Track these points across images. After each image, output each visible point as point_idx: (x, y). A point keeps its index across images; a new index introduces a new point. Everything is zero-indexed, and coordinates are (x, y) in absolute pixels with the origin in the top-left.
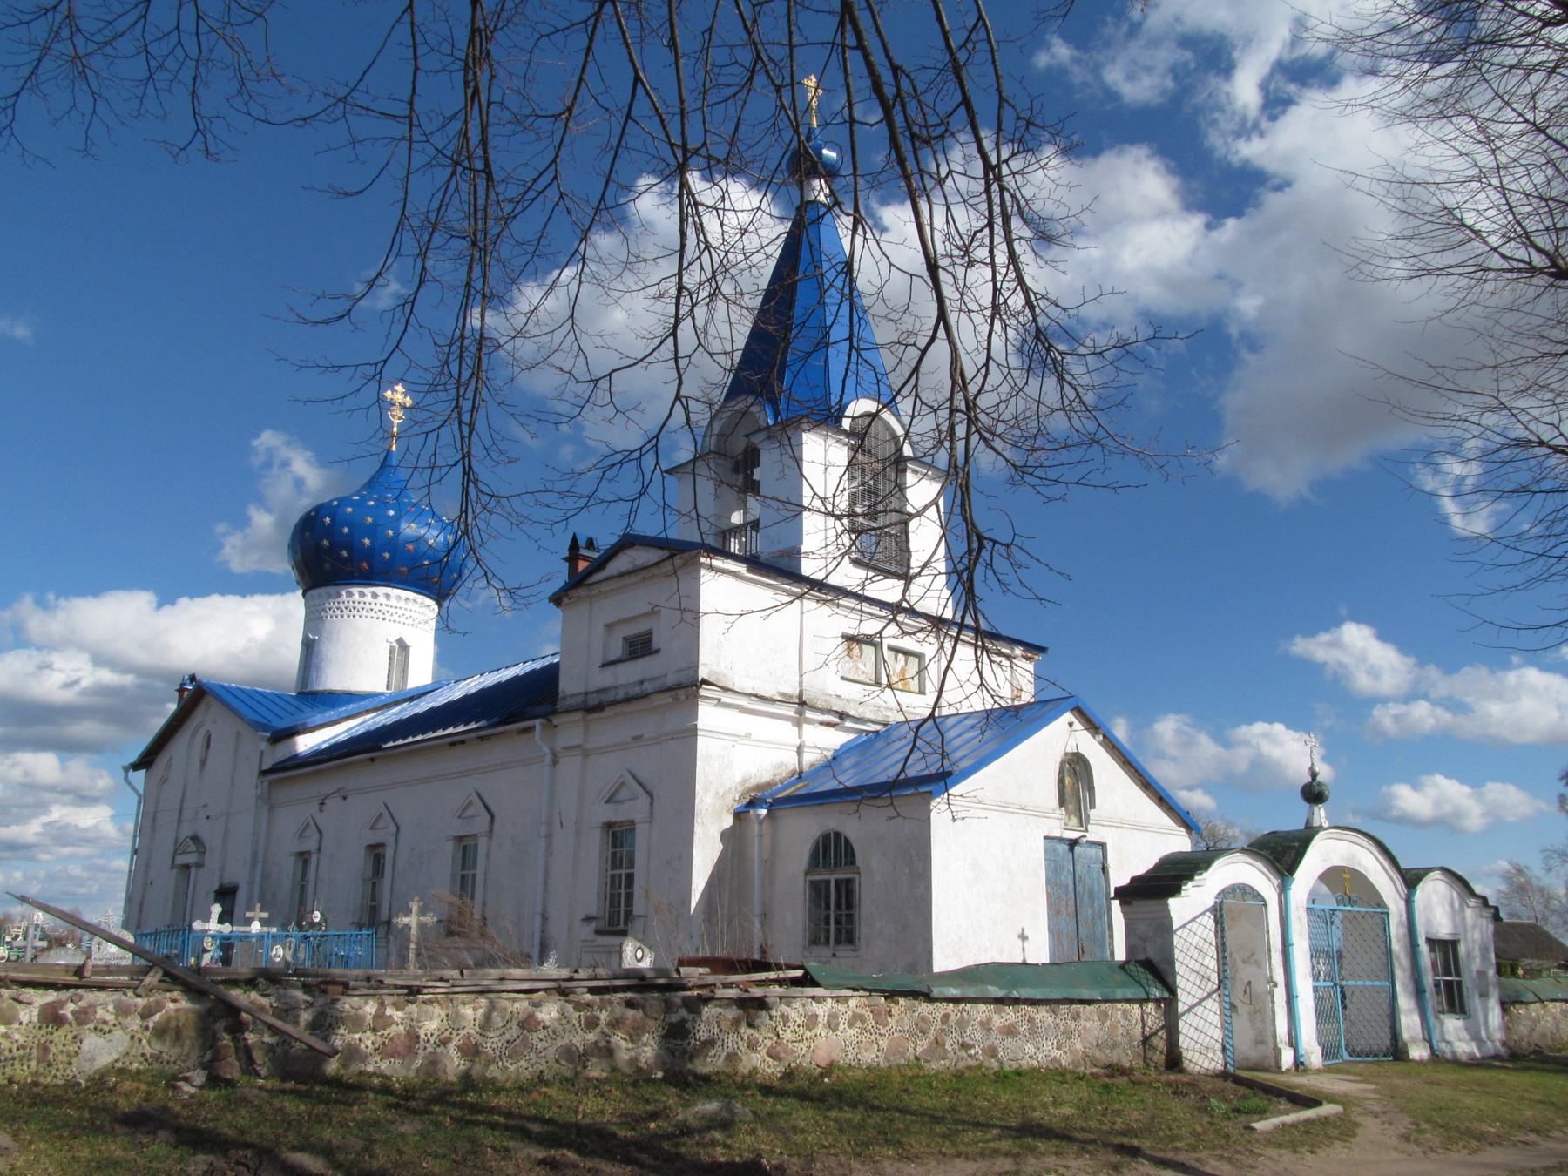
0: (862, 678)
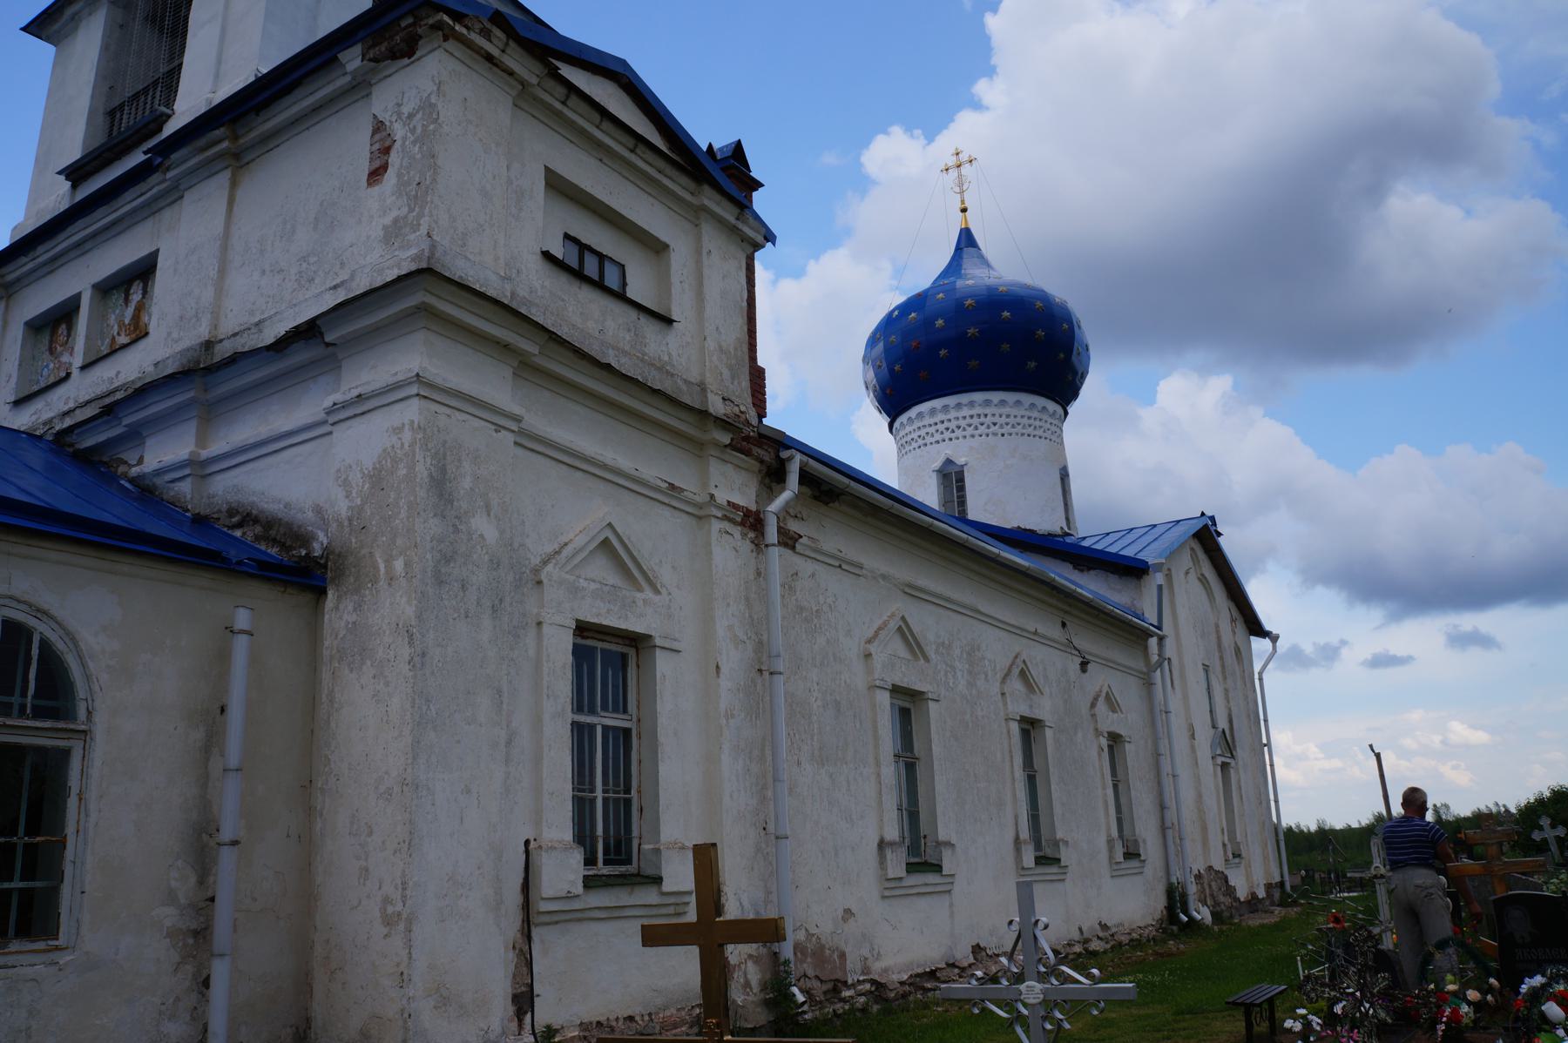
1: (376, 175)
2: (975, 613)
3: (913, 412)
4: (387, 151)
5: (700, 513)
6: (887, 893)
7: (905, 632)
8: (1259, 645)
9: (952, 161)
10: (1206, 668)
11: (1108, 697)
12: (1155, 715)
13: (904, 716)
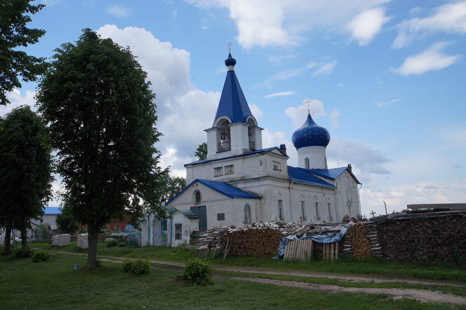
1: (261, 165)
2: (310, 191)
3: (301, 149)
5: (285, 188)
7: (303, 195)
8: (359, 186)
10: (347, 191)
13: (302, 204)
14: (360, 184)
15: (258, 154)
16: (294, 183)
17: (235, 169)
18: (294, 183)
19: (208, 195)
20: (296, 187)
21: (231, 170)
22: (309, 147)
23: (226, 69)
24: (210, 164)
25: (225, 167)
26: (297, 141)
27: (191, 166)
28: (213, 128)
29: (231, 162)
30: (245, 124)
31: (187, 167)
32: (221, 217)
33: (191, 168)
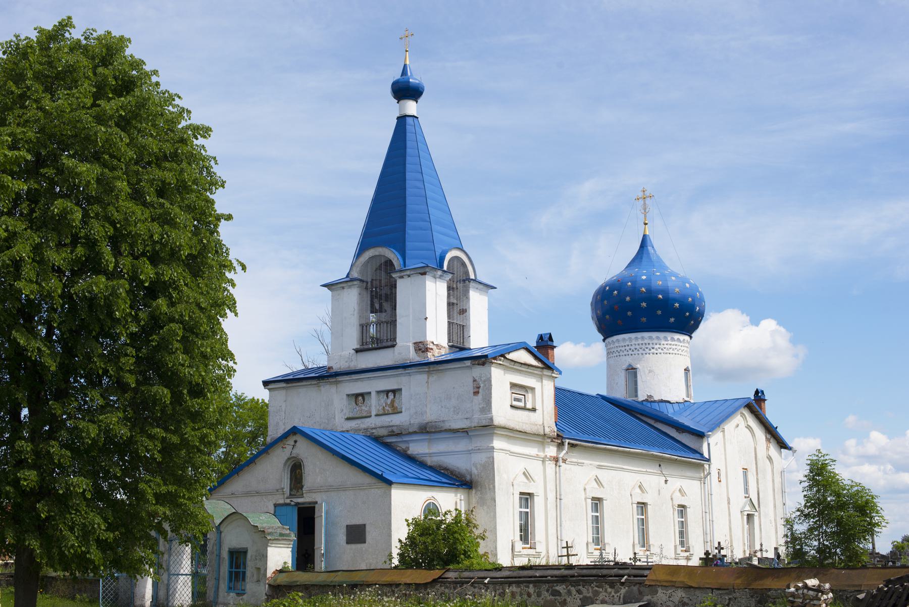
0: (364, 415)
1: (476, 393)
4: (479, 388)
6: (515, 403)
7: (597, 480)
9: (640, 195)
11: (680, 490)
12: (707, 499)
14: (790, 449)
15: (468, 363)
16: (572, 446)
17: (405, 400)
18: (572, 446)
19: (320, 472)
20: (574, 457)
21: (393, 402)
22: (639, 335)
23: (391, 109)
24: (337, 383)
25: (378, 392)
26: (604, 314)
27: (283, 385)
28: (349, 280)
29: (393, 380)
30: (439, 273)
31: (272, 386)
32: (356, 534)
33: (283, 392)
